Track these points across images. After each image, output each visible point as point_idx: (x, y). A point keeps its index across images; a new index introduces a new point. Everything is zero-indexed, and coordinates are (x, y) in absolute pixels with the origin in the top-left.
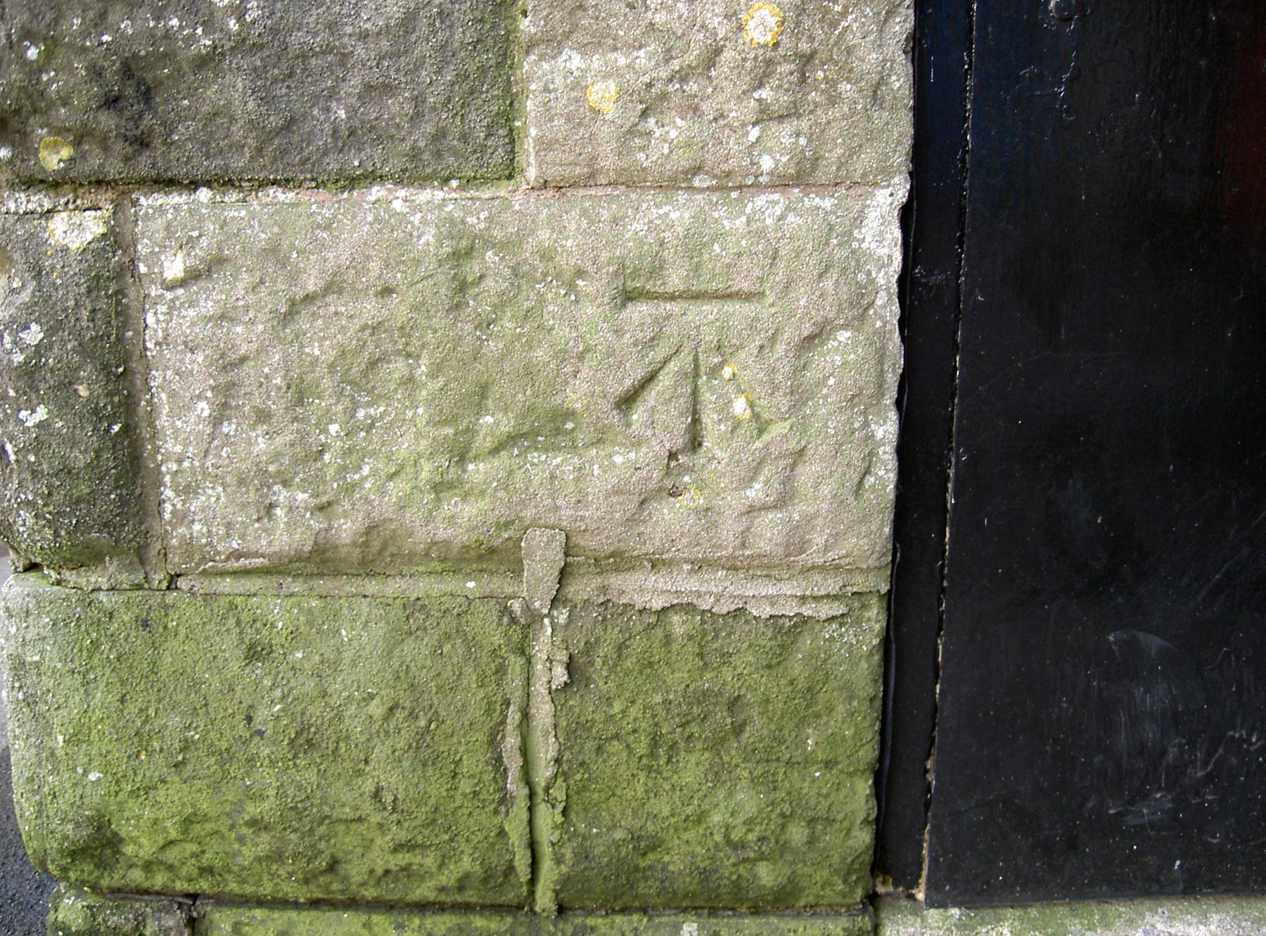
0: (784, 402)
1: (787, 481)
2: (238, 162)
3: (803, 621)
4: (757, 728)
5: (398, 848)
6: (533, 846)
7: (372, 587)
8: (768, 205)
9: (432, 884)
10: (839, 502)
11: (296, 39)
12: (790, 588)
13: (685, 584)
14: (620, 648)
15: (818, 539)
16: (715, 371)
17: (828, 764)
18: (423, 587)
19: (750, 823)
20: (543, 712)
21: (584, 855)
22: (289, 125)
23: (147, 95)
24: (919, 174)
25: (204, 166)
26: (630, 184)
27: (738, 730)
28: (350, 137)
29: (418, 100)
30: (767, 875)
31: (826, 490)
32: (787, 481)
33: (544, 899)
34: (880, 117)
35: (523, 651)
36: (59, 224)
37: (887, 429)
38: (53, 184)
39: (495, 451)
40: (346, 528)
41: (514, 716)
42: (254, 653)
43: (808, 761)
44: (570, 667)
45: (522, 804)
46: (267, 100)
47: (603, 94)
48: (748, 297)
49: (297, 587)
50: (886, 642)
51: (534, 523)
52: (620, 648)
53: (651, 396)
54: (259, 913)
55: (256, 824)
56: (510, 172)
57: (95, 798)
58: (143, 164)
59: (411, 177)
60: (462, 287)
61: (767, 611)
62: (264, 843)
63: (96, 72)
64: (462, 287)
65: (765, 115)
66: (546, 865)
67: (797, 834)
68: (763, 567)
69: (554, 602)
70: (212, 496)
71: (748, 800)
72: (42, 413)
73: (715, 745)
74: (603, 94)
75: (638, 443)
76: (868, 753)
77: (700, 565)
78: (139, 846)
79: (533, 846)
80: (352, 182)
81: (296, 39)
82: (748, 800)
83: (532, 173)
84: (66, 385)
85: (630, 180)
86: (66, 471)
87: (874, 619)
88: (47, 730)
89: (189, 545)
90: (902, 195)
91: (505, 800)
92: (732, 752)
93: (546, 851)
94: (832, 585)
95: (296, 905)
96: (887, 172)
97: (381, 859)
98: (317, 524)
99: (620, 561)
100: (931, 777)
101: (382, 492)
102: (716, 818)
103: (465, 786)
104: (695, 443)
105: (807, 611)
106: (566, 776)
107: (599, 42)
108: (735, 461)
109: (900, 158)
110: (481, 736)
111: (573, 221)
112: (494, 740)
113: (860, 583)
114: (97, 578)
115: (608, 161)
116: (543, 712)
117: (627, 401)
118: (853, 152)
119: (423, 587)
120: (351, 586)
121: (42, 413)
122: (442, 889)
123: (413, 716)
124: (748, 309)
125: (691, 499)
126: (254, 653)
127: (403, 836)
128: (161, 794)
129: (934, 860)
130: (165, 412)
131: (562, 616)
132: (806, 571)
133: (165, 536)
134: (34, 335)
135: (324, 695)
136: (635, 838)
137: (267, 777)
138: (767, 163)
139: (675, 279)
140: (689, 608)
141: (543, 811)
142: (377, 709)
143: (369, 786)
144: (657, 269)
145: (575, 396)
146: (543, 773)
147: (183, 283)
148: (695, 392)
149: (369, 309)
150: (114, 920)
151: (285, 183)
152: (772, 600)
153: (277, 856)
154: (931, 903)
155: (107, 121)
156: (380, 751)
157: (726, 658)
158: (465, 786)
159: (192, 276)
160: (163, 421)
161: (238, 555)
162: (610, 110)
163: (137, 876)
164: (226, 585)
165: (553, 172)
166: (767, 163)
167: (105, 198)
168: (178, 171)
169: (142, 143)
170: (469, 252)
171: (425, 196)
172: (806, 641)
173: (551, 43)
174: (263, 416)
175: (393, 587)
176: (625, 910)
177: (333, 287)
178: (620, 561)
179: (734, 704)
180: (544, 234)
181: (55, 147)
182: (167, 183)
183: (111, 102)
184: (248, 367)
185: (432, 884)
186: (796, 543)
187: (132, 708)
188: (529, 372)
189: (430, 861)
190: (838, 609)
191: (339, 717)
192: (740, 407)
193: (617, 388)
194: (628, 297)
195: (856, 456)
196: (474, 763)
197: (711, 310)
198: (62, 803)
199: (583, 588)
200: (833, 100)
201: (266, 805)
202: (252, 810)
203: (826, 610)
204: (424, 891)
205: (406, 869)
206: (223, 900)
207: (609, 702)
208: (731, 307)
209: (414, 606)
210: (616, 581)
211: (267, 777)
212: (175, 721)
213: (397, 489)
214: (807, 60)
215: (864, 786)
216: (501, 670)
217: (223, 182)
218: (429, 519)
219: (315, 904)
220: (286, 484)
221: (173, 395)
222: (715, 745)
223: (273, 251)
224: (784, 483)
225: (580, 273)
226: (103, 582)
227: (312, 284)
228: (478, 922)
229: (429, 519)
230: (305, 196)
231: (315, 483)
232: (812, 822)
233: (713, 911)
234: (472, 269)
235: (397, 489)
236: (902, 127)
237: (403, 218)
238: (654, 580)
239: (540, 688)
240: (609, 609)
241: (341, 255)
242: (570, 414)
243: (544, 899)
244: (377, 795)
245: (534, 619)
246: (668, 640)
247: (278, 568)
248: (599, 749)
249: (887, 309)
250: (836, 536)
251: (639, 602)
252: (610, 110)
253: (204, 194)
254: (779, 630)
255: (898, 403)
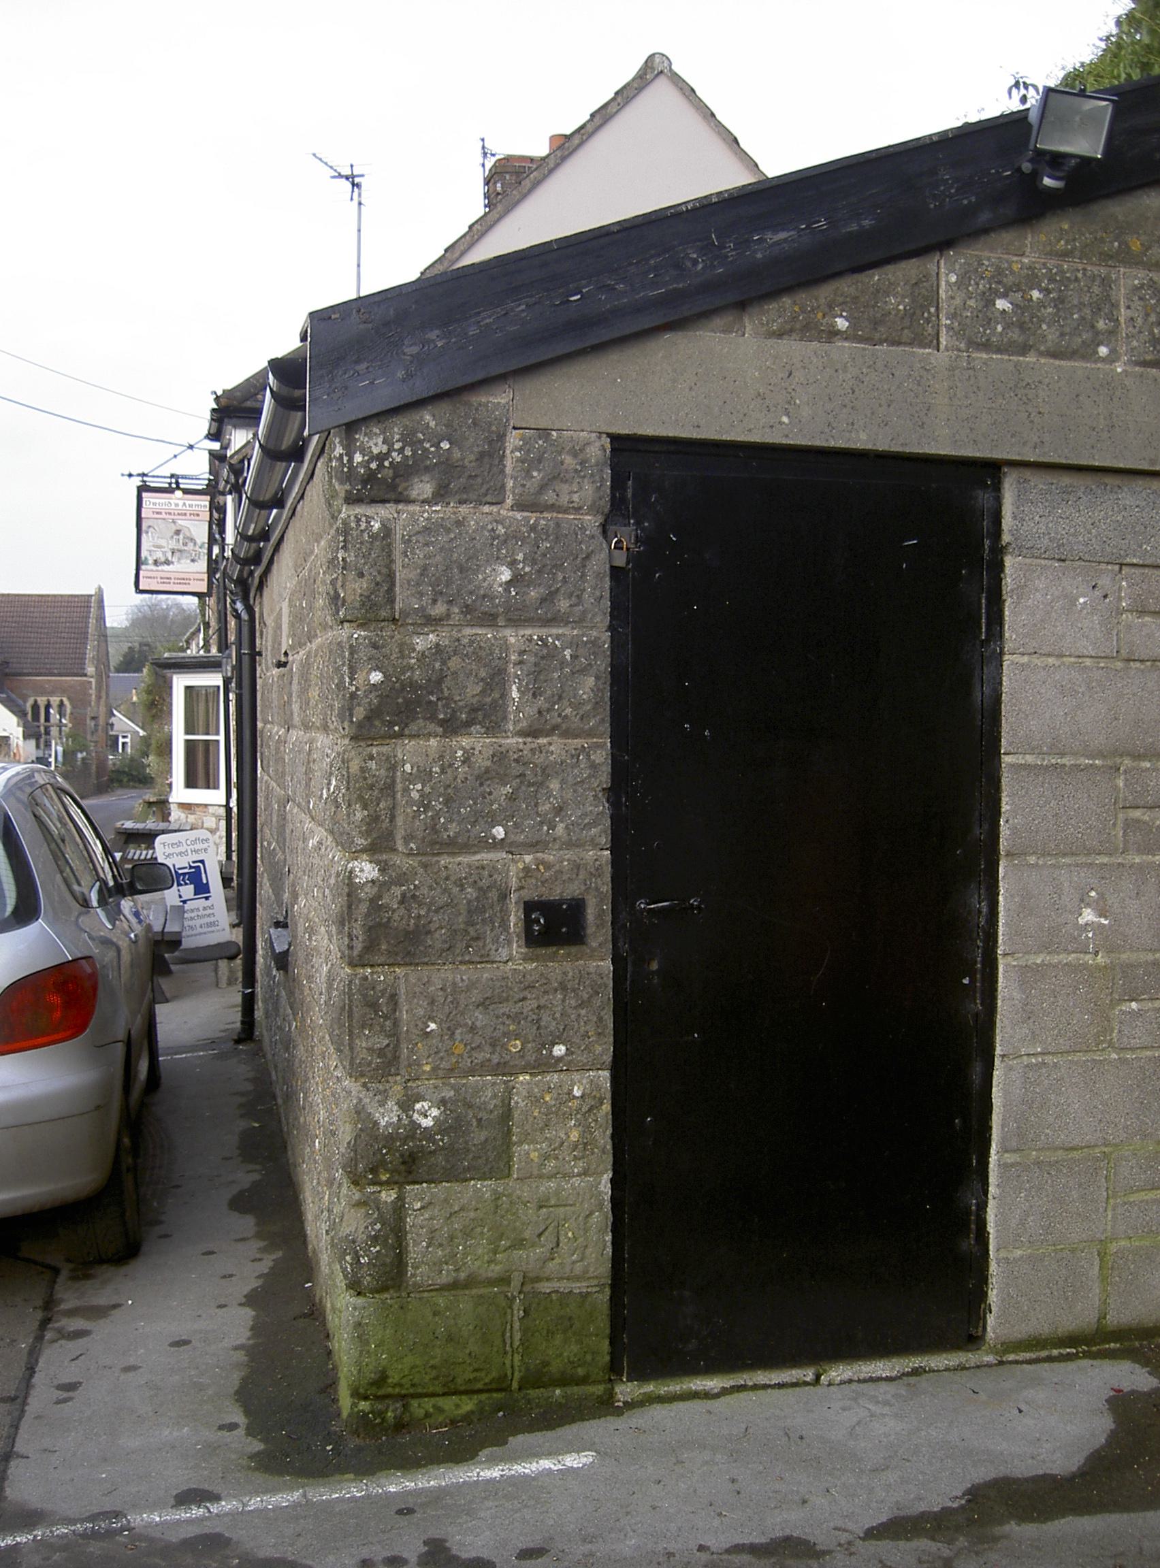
0: (582, 1233)
1: (583, 1254)
2: (436, 1177)
3: (588, 1293)
4: (577, 1325)
5: (476, 1370)
6: (512, 1367)
7: (467, 1292)
8: (576, 1181)
9: (482, 1382)
10: (597, 1259)
11: (456, 1146)
12: (584, 1284)
13: (555, 1285)
14: (538, 1304)
15: (592, 1269)
16: (563, 1225)
17: (597, 1335)
18: (482, 1291)
19: (575, 1355)
20: (517, 1325)
21: (528, 1369)
22: (453, 1167)
23: (414, 1161)
24: (615, 1171)
25: (427, 1178)
26: (540, 1177)
27: (571, 1326)
28: (468, 1169)
29: (487, 1160)
30: (581, 1371)
31: (593, 1255)
32: (583, 1254)
33: (515, 1385)
34: (604, 1157)
35: (511, 1307)
36: (383, 1194)
37: (609, 1238)
38: (381, 1184)
39: (505, 1251)
40: (463, 1275)
41: (509, 1327)
42: (435, 1314)
43: (591, 1335)
44: (524, 1311)
45: (510, 1353)
46: (447, 1161)
47: (534, 1155)
48: (571, 1205)
49: (446, 1294)
50: (611, 1298)
51: (515, 1270)
52: (538, 1304)
53: (546, 1233)
54: (426, 1399)
55: (433, 1367)
56: (509, 1175)
57: (384, 1363)
58: (410, 1178)
59: (483, 1178)
60: (497, 1207)
61: (578, 1291)
62: (434, 1373)
63: (402, 1156)
64: (497, 1207)
65: (575, 1158)
66: (516, 1374)
67: (589, 1357)
68: (578, 1278)
69: (520, 1293)
70: (423, 1269)
71: (575, 1348)
72: (378, 1248)
73: (565, 1331)
74: (534, 1155)
75: (543, 1246)
76: (608, 1331)
77: (560, 1279)
78: (394, 1378)
79: (512, 1367)
80: (466, 1180)
81: (456, 1146)
82: (575, 1348)
83: (515, 1176)
84: (386, 1240)
85: (540, 1176)
86: (384, 1264)
87: (608, 1291)
88: (368, 1343)
89: (415, 1284)
90: (611, 1176)
91: (506, 1353)
92: (570, 1334)
93: (517, 1368)
94: (595, 1282)
95: (438, 1395)
96: (607, 1171)
97: (469, 1375)
98: (454, 1275)
99: (538, 1279)
100: (625, 1340)
101: (473, 1264)
102: (565, 1354)
103: (495, 1349)
104: (558, 1245)
105: (589, 1290)
106: (523, 1344)
107: (534, 1142)
108: (569, 1249)
109: (610, 1167)
110: (499, 1334)
111: (526, 1188)
112: (503, 1335)
113: (603, 1281)
114: (386, 1295)
115: (536, 1172)
116: (517, 1325)
117: (540, 1235)
118: (598, 1166)
119: (482, 1291)
120: (462, 1292)
121: (378, 1248)
122: (486, 1384)
123: (481, 1329)
124: (573, 1208)
125: (557, 1261)
126: (435, 1314)
127: (476, 1366)
128: (405, 1360)
129: (628, 1366)
130: (1061, 1351)
131: (522, 1297)
132: (589, 1278)
133: (407, 1282)
134: (378, 1226)
135: (456, 1324)
136: (543, 1362)
137: (438, 1351)
138: (576, 1170)
139: (553, 1202)
140: (557, 1292)
141: (516, 1355)
142: (471, 1327)
143: (467, 1351)
144: (548, 1200)
145: (527, 1235)
146: (517, 1343)
147: (419, 1210)
148: (558, 1232)
149: (472, 1214)
150: (380, 1407)
151: (447, 1182)
152: (579, 1288)
153: (436, 1378)
154: (628, 1381)
155: (402, 1168)
156: (472, 1340)
157: (568, 1305)
158: (495, 1349)
159: (422, 1208)
160: (410, 1248)
161: (430, 1285)
162: (536, 1160)
163: (390, 1390)
164: (426, 1294)
165: (520, 1176)
166: (576, 1170)
167: (396, 1187)
168: (420, 1180)
169: (410, 1173)
170: (498, 1198)
171: (486, 1183)
172: (590, 1299)
173: (520, 1143)
174: (441, 1245)
175: (474, 1291)
176: (538, 1388)
177: (462, 1209)
178: (538, 1279)
179: (570, 1318)
180: (518, 1192)
181: (384, 1175)
182: (414, 1183)
183: (404, 1163)
184: (437, 1232)
185: (482, 1382)
186: (586, 1271)
187: (399, 1333)
188: (515, 1229)
189: (483, 1374)
190: (597, 1289)
191: (460, 1331)
192: (570, 1234)
193: (537, 1232)
194: (541, 1207)
195: (601, 1246)
196: (498, 1342)
197: (562, 1209)
198: (371, 1367)
199: (527, 1288)
200: (593, 1153)
201: (437, 1360)
202: (432, 1362)
203: (594, 1290)
204: (479, 1386)
205: (475, 1378)
206: (413, 1396)
207: (535, 1320)
208: (567, 1208)
209: (481, 1296)
210: (536, 1285)
211: (438, 1351)
212: (411, 1336)
213: (478, 1263)
214: (585, 1144)
215: (607, 1342)
216: (505, 1313)
217: (429, 1182)
218: (486, 1271)
219: (444, 1394)
220: (447, 1264)
221: (414, 1241)
222: (565, 1331)
223: (446, 1200)
224: (491, 442)
225: (528, 1202)
226: (388, 1296)
227: (456, 1208)
228: (495, 1395)
229: (486, 1271)
230: (453, 1184)
231: (454, 1264)
232: (593, 1353)
233: (564, 1386)
234: (500, 1202)
235: (478, 1263)
236: (610, 1159)
237: (480, 1189)
238: (546, 1284)
239: (516, 1318)
240: (536, 1294)
241: (464, 1201)
242: (525, 1240)
243: (515, 1385)
244: (470, 1354)
245: (514, 1298)
246: (551, 1301)
247: (443, 1288)
248: (532, 1335)
249: (608, 1206)
250: (596, 1269)
251: (543, 1291)
252: (536, 1160)
253: (425, 1185)
254: (582, 1296)
255: (612, 1231)
